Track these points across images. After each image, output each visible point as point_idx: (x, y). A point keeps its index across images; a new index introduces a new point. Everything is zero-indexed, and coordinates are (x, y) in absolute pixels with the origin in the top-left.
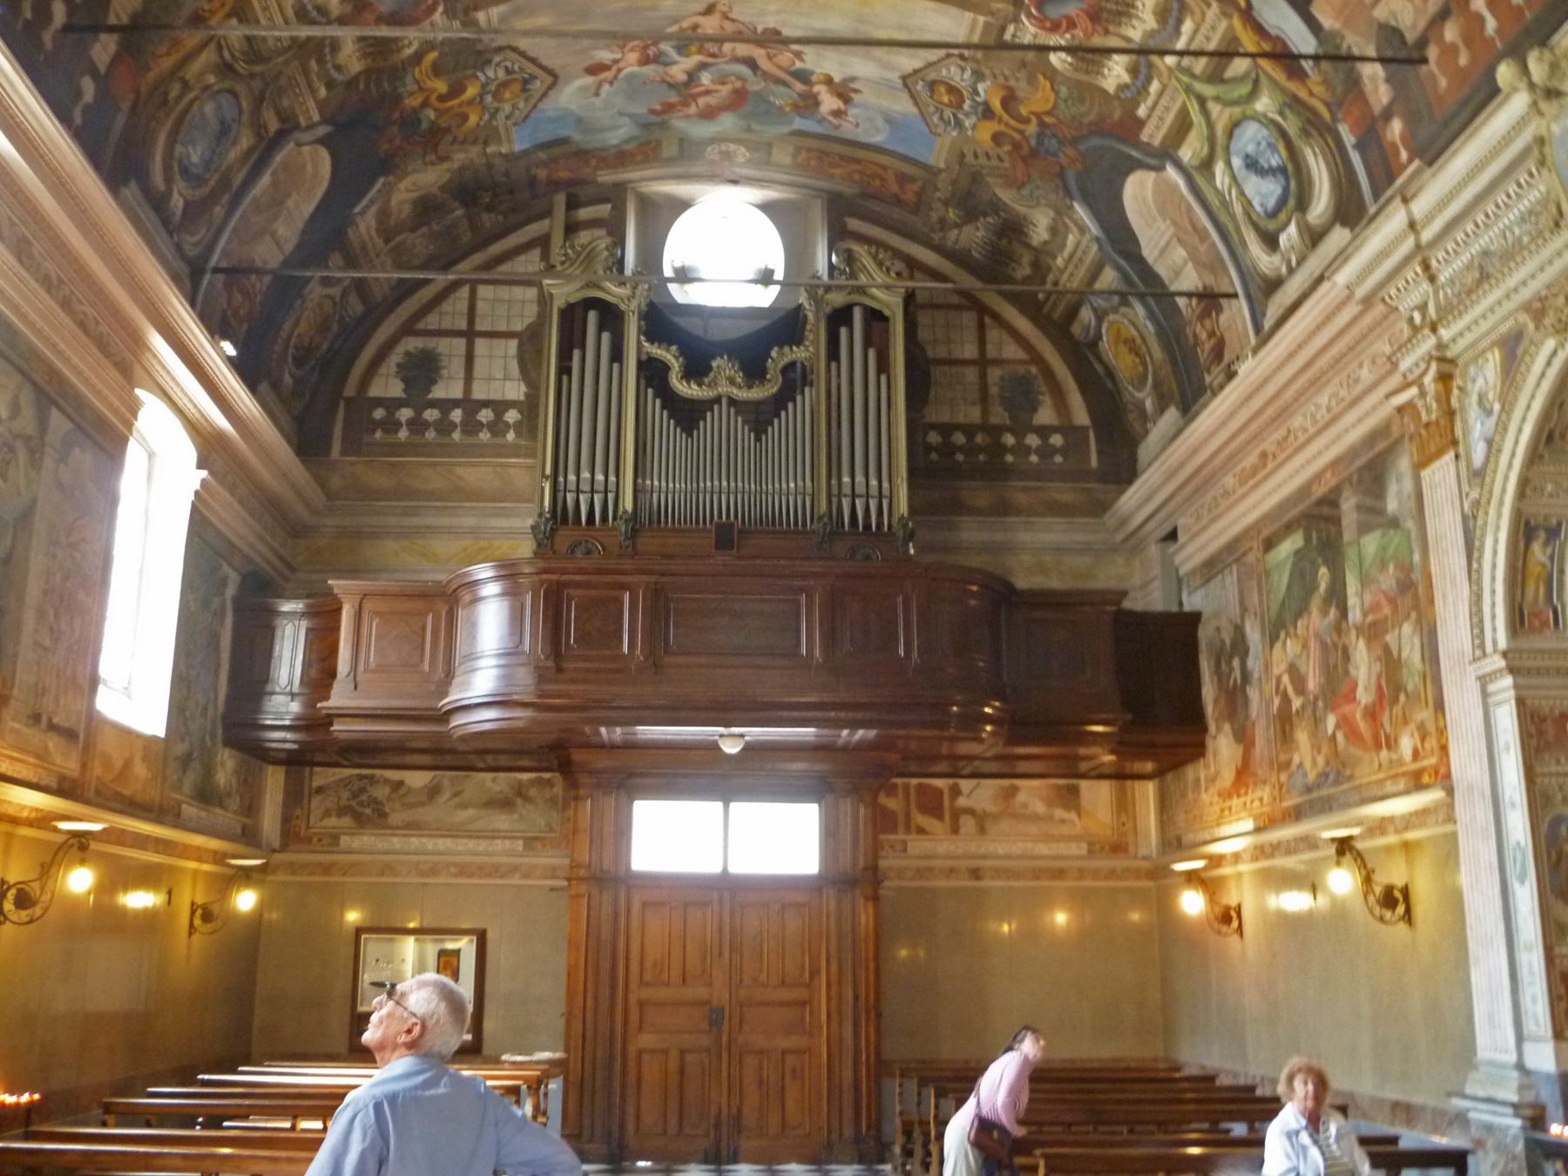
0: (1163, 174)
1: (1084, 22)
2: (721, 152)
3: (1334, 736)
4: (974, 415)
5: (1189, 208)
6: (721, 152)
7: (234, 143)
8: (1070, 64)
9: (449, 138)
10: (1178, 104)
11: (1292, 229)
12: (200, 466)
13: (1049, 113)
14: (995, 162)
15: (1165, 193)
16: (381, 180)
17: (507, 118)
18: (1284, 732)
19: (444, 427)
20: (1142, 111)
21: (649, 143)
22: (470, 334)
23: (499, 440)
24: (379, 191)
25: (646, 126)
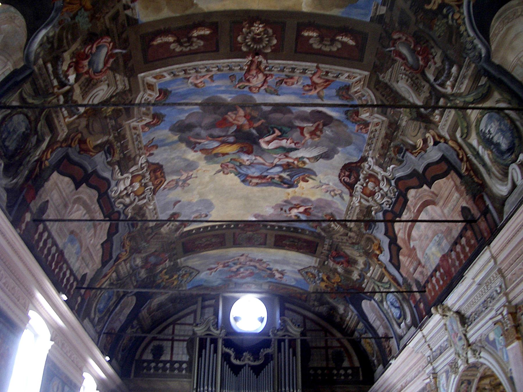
4: (324, 364)
10: (372, 286)
19: (164, 369)
20: (363, 286)
22: (173, 340)
23: (180, 373)
25: (225, 281)
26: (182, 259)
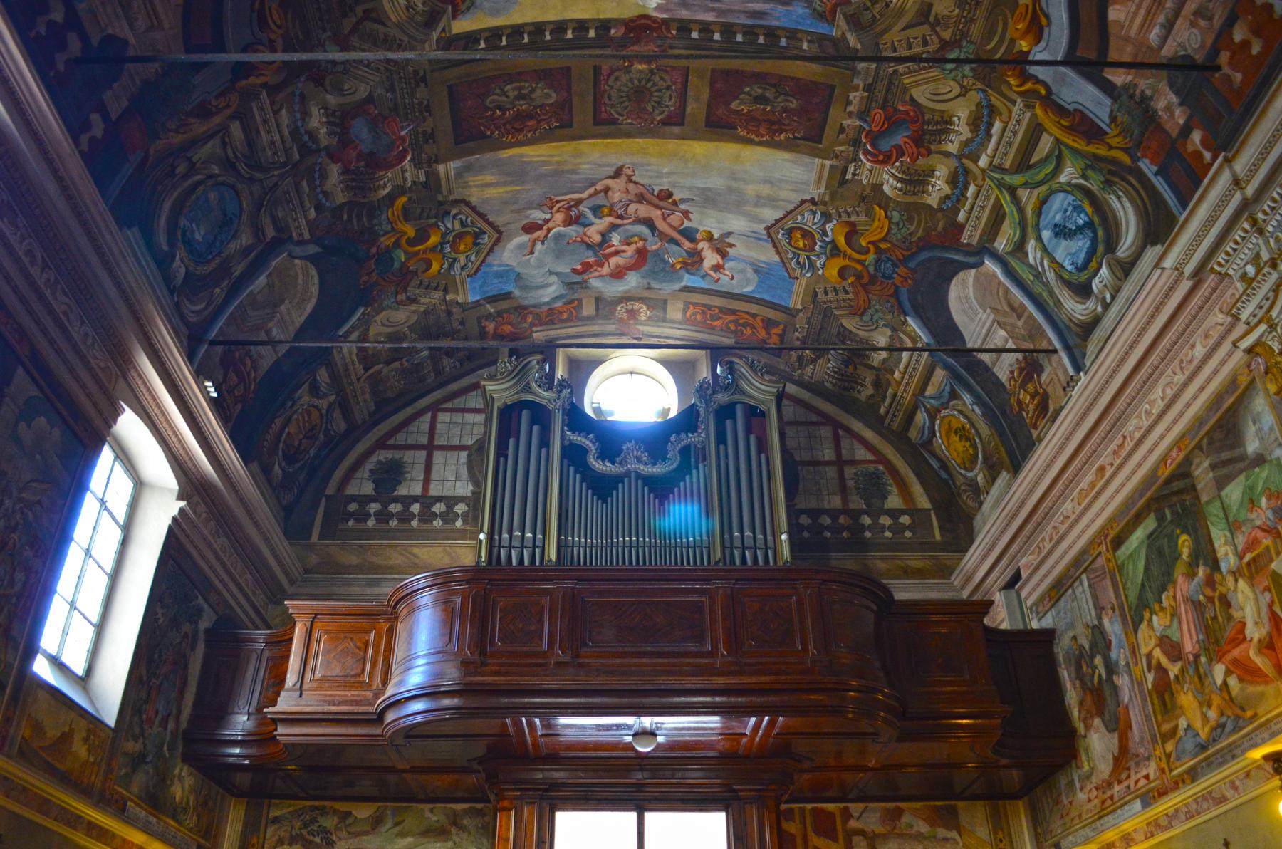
0: (982, 269)
1: (911, 149)
2: (628, 311)
3: (1225, 683)
4: (836, 502)
5: (1007, 290)
6: (628, 311)
7: (235, 236)
8: (900, 190)
9: (415, 282)
10: (992, 200)
11: (1104, 271)
12: (180, 497)
13: (884, 240)
14: (842, 296)
15: (986, 287)
16: (362, 309)
17: (463, 268)
18: (1164, 704)
19: (405, 517)
20: (961, 217)
21: (572, 302)
22: (430, 448)
24: (359, 319)
25: (570, 285)
26: (453, 165)
